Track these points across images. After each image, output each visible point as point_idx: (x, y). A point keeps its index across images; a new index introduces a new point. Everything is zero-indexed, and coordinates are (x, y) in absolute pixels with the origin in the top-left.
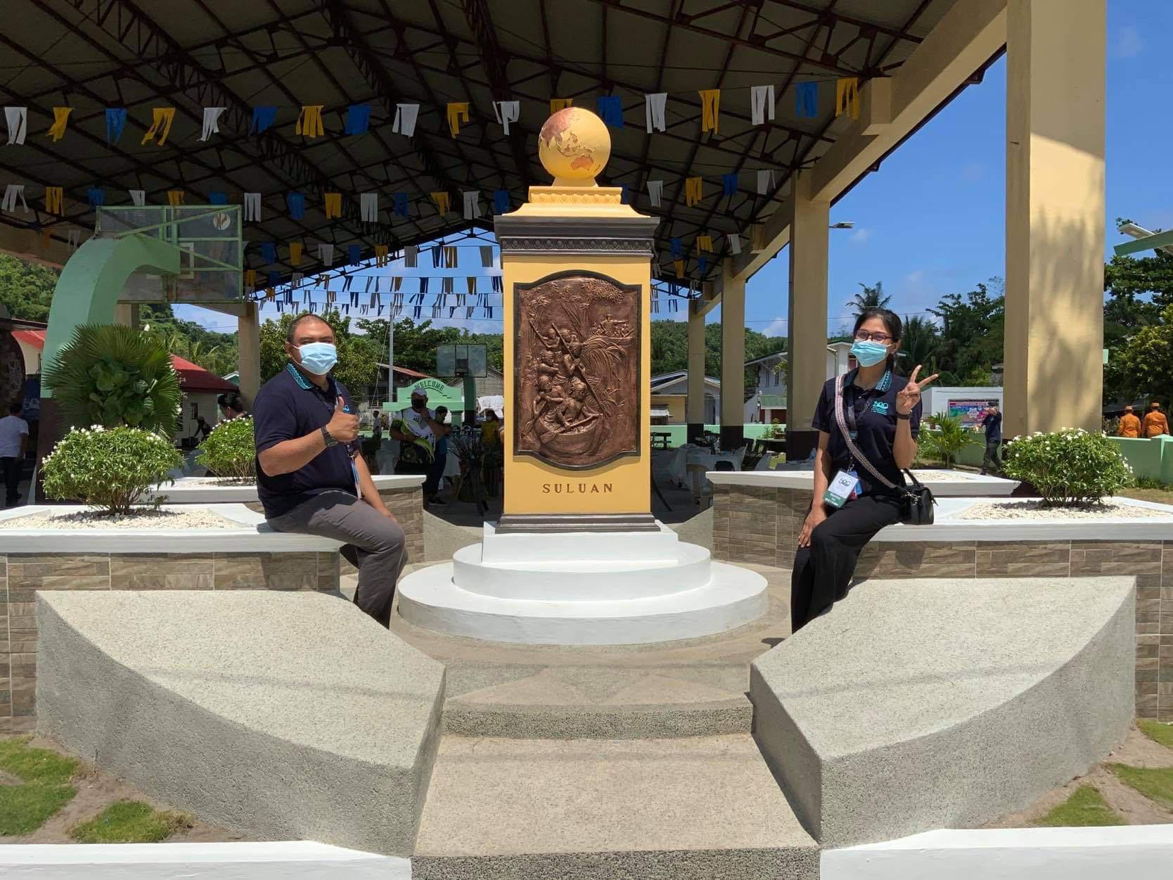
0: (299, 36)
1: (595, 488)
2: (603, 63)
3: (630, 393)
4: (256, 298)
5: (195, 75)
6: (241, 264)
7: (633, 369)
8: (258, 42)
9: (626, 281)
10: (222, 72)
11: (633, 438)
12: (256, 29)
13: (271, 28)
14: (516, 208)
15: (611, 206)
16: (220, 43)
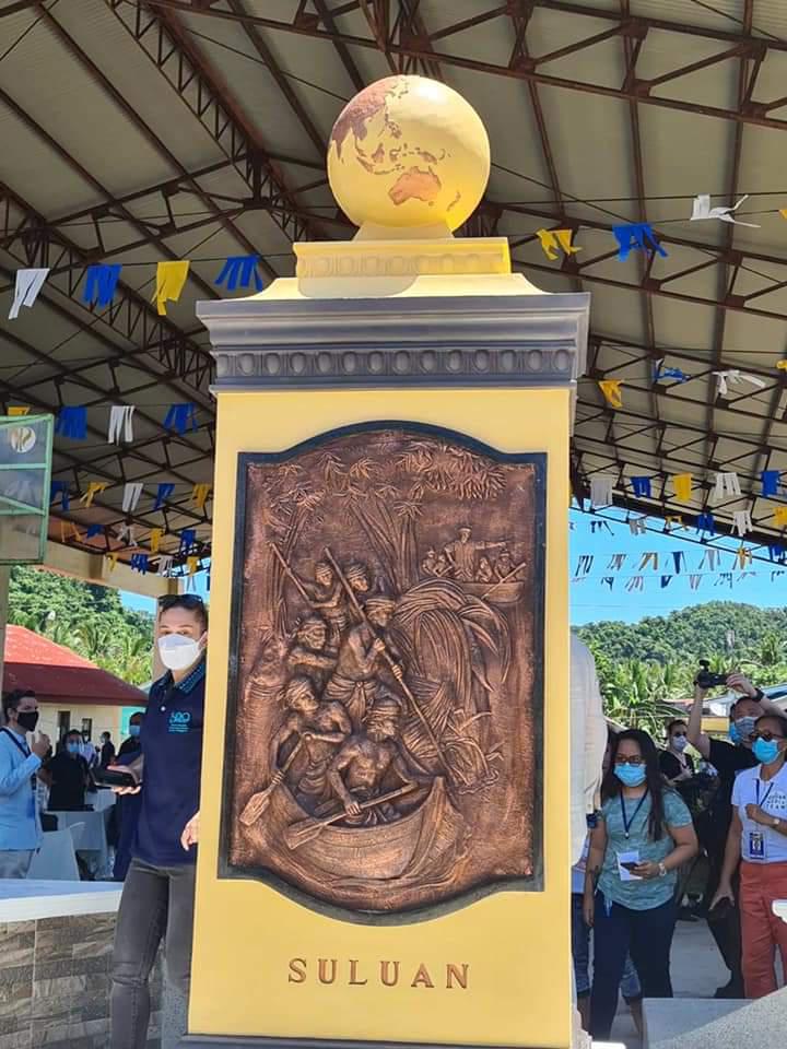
0: (207, 198)
1: (422, 978)
2: (639, 197)
3: (516, 725)
4: (181, 574)
5: (67, 257)
6: (46, 505)
7: (523, 663)
8: (151, 208)
9: (506, 443)
10: (99, 252)
11: (525, 842)
12: (148, 192)
13: (168, 189)
14: (260, 288)
15: (490, 275)
16: (98, 213)
